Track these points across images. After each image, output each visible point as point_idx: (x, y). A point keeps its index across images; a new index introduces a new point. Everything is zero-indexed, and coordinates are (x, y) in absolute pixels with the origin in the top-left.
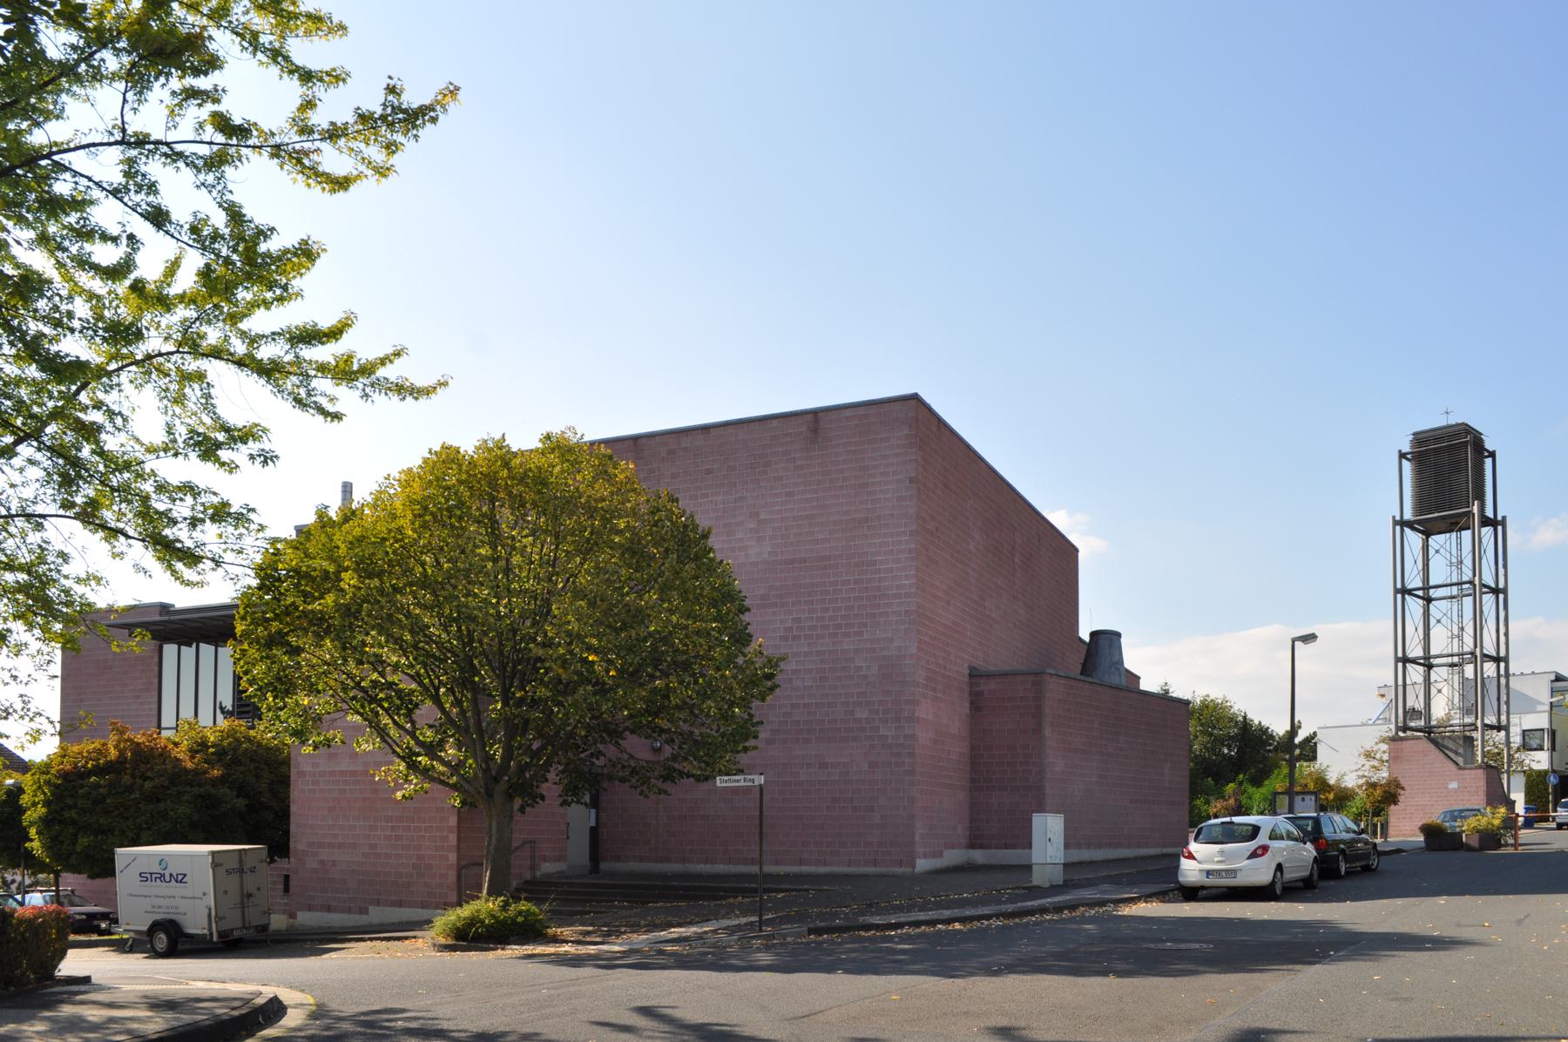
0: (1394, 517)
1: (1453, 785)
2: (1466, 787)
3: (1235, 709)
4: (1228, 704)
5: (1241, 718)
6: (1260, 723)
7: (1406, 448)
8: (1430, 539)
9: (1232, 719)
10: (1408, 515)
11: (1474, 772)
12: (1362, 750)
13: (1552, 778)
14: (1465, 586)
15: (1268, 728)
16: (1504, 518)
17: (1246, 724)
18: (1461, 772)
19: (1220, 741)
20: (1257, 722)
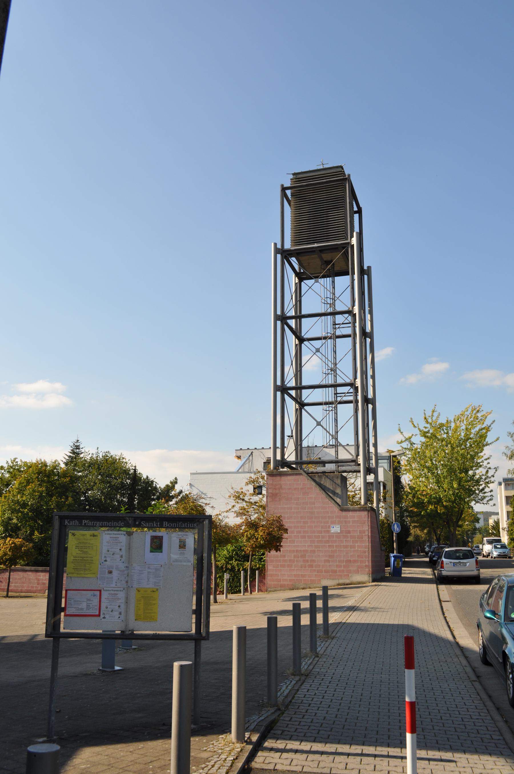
0: (275, 244)
1: (336, 529)
2: (349, 532)
3: (128, 466)
4: (124, 460)
5: (132, 471)
6: (147, 477)
7: (288, 184)
8: (302, 283)
9: (126, 472)
10: (288, 245)
11: (358, 513)
12: (232, 491)
13: (396, 526)
14: (339, 319)
15: (152, 482)
16: (369, 268)
17: (135, 477)
18: (344, 514)
19: (116, 489)
20: (145, 477)
